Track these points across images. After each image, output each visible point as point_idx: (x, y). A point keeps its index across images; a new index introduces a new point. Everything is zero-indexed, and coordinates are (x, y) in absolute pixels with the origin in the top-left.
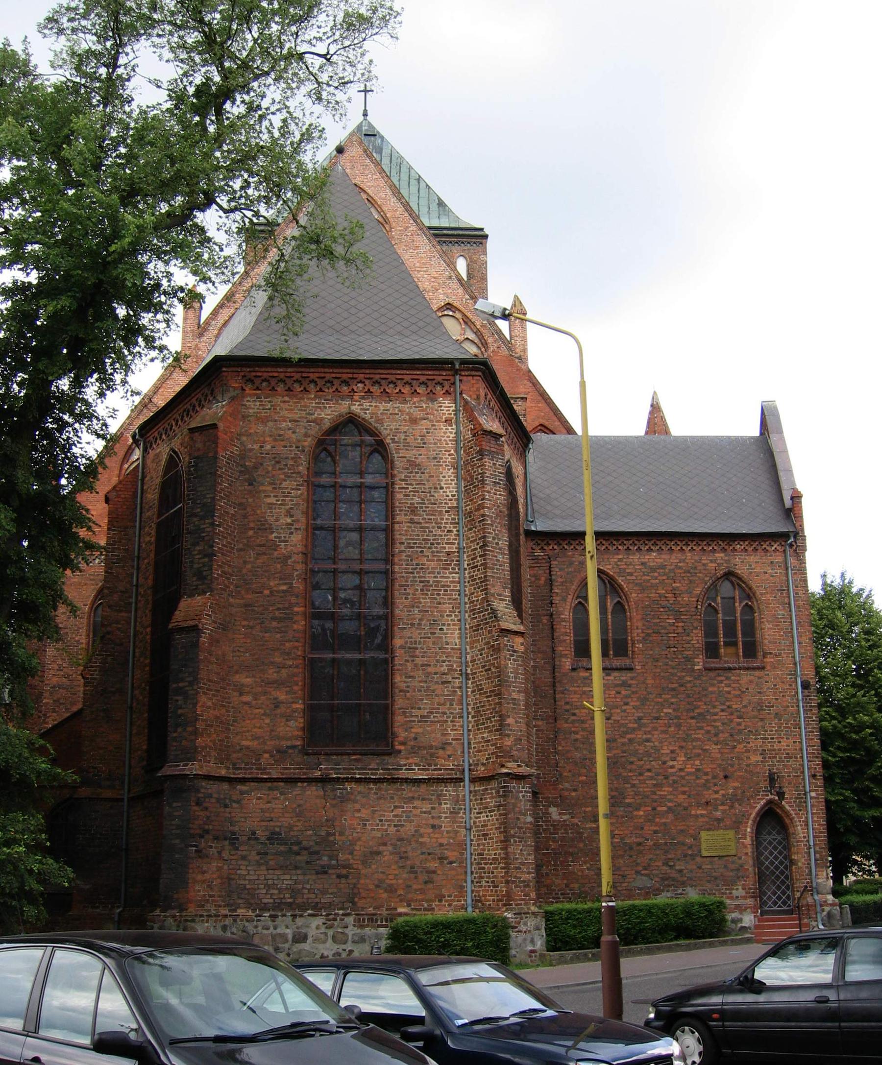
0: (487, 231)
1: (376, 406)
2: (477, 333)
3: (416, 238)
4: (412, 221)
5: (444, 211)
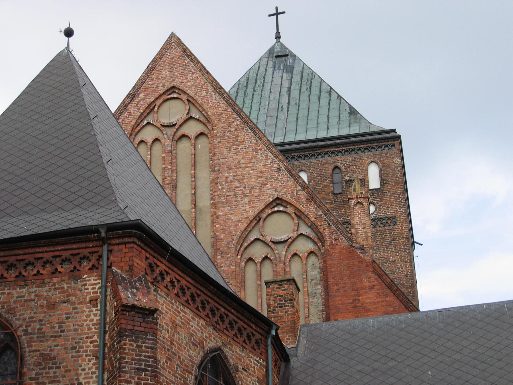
0: (399, 132)
1: (9, 294)
2: (312, 226)
3: (240, 133)
4: (235, 116)
5: (356, 118)
